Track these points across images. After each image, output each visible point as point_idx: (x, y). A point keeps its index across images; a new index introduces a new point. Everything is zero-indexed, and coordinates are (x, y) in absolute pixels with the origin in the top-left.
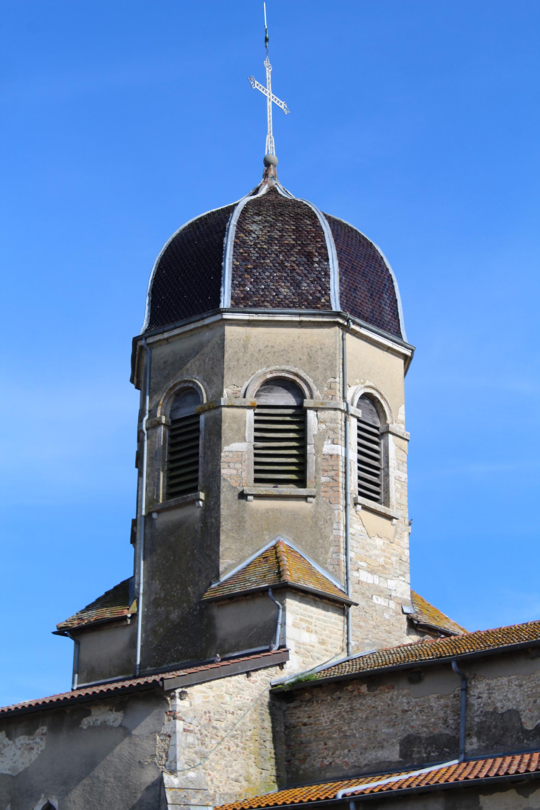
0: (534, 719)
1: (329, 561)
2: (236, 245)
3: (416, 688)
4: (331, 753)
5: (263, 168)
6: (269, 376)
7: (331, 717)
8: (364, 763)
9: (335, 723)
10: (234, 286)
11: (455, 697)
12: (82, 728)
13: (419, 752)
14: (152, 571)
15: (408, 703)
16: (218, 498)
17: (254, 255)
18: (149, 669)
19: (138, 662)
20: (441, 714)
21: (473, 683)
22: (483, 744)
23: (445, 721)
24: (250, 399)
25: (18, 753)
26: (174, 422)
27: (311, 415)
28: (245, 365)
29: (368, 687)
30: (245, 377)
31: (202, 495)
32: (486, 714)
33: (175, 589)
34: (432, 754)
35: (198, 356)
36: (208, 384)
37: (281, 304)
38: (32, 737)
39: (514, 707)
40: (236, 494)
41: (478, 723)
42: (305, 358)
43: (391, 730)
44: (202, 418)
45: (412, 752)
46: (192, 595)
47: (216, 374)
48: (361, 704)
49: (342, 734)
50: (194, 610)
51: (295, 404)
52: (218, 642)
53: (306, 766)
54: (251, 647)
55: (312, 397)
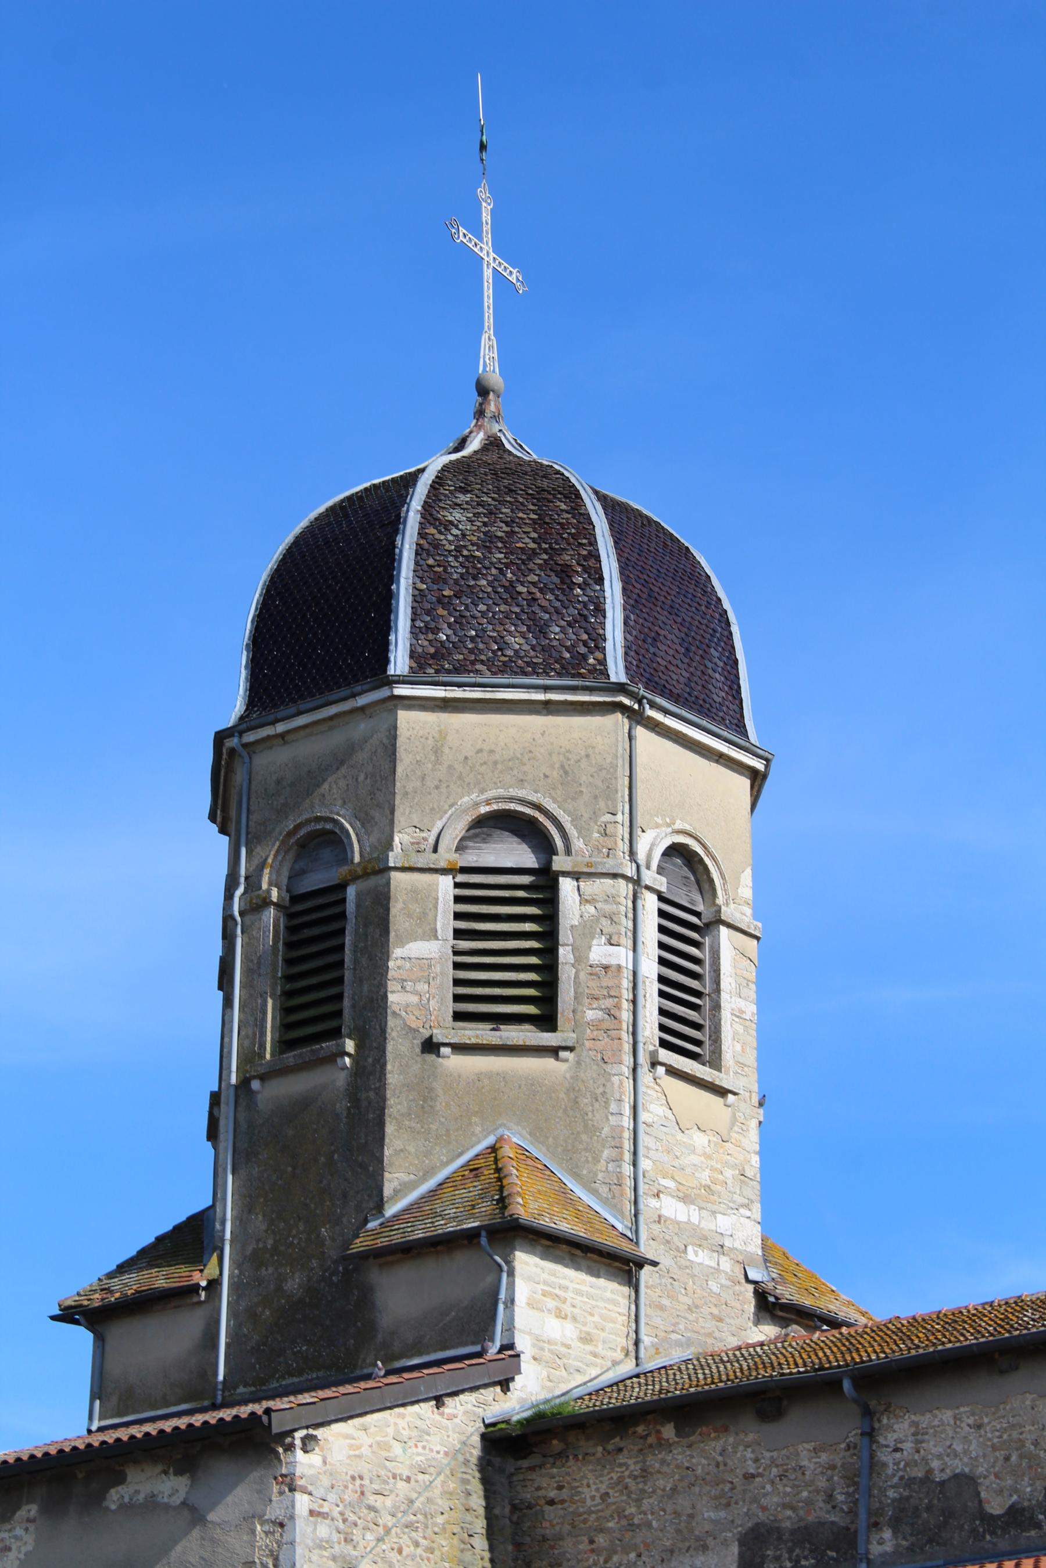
1: (600, 1176)
3: (774, 1431)
5: (475, 398)
6: (484, 809)
7: (603, 1488)
9: (611, 1500)
12: (107, 1509)
14: (250, 1196)
17: (456, 570)
18: (241, 1389)
19: (221, 1378)
20: (822, 1483)
21: (885, 1421)
22: (904, 1543)
23: (830, 1497)
24: (447, 856)
26: (295, 899)
27: (567, 886)
28: (437, 787)
30: (436, 812)
31: (350, 1046)
33: (294, 1232)
34: (803, 1563)
35: (343, 770)
36: (363, 826)
37: (509, 667)
40: (418, 1042)
41: (894, 1500)
42: (555, 774)
43: (722, 1514)
46: (328, 1242)
47: (378, 805)
48: (663, 1462)
49: (624, 1522)
50: (333, 1274)
51: (536, 866)
55: (568, 852)
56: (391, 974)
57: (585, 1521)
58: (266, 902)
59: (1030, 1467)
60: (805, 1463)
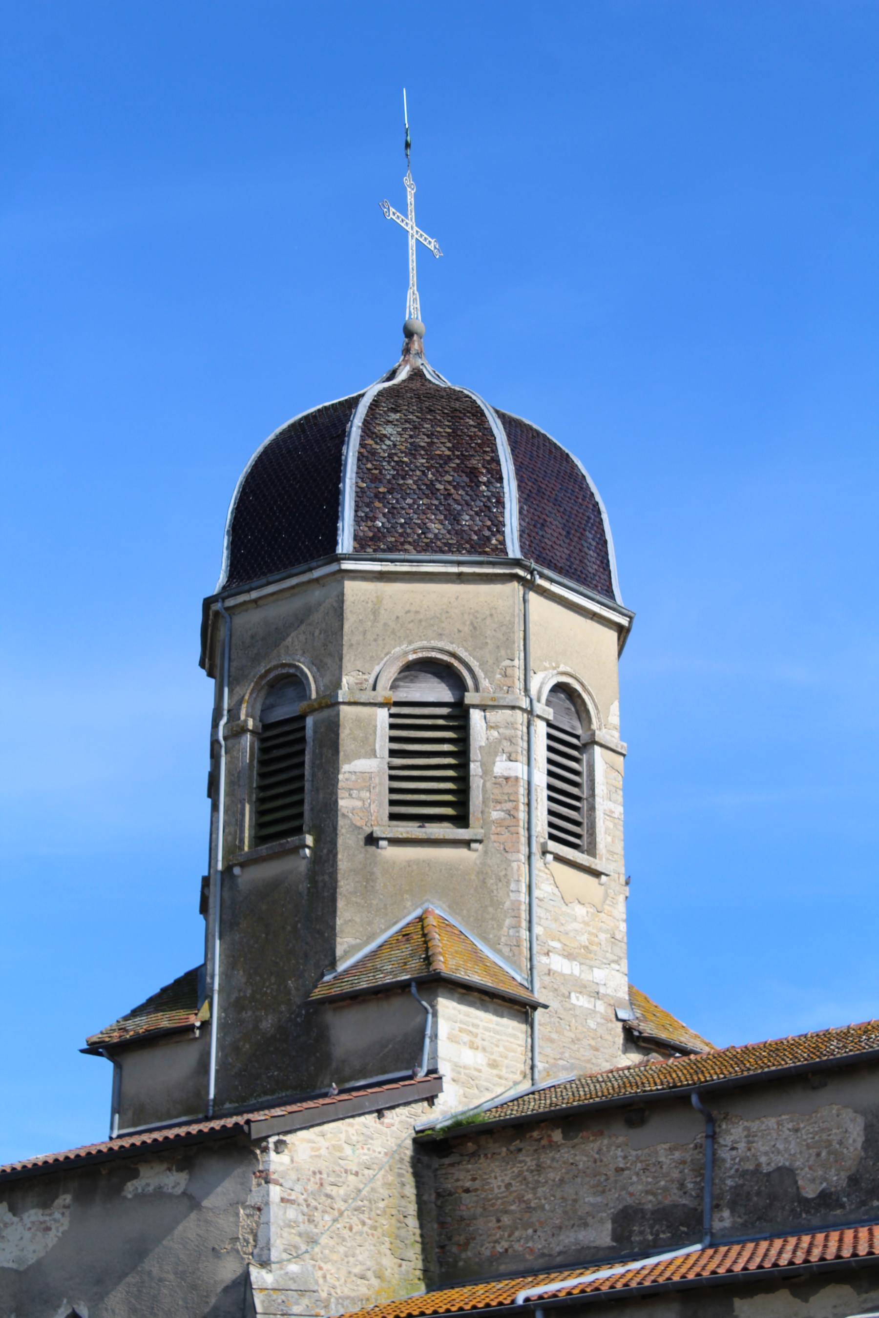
0: (818, 1182)
1: (503, 939)
2: (361, 458)
4: (506, 1234)
6: (412, 657)
7: (507, 1180)
8: (558, 1249)
10: (358, 520)
11: (696, 1147)
12: (125, 1198)
13: (641, 1233)
14: (233, 956)
15: (625, 1157)
16: (334, 843)
17: (389, 472)
18: (227, 1105)
19: (212, 1096)
20: (676, 1174)
21: (724, 1126)
22: (739, 1220)
23: (682, 1186)
24: (383, 693)
25: (28, 1235)
26: (266, 727)
27: (476, 716)
28: (375, 640)
29: (563, 1132)
31: (309, 840)
32: (743, 1174)
33: (267, 984)
34: (662, 1236)
35: (303, 627)
36: (318, 670)
37: (430, 546)
38: (48, 1211)
39: (787, 1164)
40: (362, 837)
41: (731, 1187)
42: (467, 629)
43: (599, 1199)
44: (310, 721)
45: (631, 1232)
46: (293, 992)
48: (553, 1159)
49: (523, 1206)
51: (452, 700)
52: (334, 1065)
53: (469, 1254)
54: (384, 1072)
55: (477, 689)
56: (340, 785)
57: (493, 1205)
58: (243, 730)
59: (836, 1161)
60: (662, 1159)
